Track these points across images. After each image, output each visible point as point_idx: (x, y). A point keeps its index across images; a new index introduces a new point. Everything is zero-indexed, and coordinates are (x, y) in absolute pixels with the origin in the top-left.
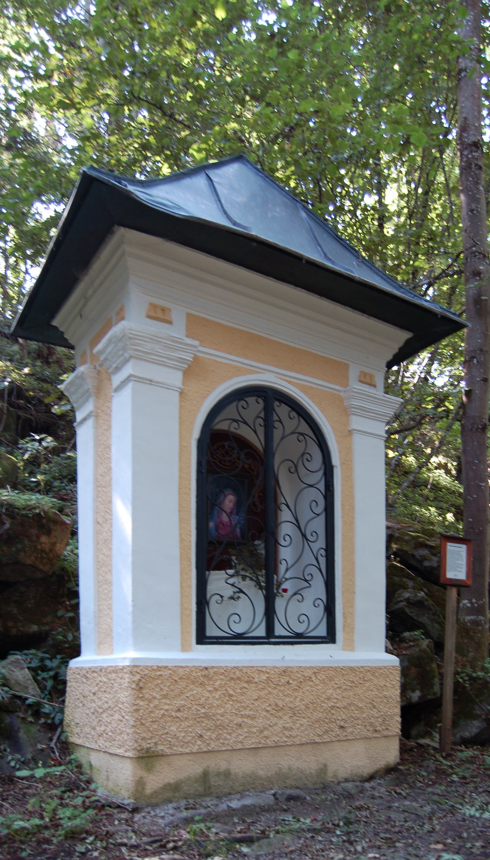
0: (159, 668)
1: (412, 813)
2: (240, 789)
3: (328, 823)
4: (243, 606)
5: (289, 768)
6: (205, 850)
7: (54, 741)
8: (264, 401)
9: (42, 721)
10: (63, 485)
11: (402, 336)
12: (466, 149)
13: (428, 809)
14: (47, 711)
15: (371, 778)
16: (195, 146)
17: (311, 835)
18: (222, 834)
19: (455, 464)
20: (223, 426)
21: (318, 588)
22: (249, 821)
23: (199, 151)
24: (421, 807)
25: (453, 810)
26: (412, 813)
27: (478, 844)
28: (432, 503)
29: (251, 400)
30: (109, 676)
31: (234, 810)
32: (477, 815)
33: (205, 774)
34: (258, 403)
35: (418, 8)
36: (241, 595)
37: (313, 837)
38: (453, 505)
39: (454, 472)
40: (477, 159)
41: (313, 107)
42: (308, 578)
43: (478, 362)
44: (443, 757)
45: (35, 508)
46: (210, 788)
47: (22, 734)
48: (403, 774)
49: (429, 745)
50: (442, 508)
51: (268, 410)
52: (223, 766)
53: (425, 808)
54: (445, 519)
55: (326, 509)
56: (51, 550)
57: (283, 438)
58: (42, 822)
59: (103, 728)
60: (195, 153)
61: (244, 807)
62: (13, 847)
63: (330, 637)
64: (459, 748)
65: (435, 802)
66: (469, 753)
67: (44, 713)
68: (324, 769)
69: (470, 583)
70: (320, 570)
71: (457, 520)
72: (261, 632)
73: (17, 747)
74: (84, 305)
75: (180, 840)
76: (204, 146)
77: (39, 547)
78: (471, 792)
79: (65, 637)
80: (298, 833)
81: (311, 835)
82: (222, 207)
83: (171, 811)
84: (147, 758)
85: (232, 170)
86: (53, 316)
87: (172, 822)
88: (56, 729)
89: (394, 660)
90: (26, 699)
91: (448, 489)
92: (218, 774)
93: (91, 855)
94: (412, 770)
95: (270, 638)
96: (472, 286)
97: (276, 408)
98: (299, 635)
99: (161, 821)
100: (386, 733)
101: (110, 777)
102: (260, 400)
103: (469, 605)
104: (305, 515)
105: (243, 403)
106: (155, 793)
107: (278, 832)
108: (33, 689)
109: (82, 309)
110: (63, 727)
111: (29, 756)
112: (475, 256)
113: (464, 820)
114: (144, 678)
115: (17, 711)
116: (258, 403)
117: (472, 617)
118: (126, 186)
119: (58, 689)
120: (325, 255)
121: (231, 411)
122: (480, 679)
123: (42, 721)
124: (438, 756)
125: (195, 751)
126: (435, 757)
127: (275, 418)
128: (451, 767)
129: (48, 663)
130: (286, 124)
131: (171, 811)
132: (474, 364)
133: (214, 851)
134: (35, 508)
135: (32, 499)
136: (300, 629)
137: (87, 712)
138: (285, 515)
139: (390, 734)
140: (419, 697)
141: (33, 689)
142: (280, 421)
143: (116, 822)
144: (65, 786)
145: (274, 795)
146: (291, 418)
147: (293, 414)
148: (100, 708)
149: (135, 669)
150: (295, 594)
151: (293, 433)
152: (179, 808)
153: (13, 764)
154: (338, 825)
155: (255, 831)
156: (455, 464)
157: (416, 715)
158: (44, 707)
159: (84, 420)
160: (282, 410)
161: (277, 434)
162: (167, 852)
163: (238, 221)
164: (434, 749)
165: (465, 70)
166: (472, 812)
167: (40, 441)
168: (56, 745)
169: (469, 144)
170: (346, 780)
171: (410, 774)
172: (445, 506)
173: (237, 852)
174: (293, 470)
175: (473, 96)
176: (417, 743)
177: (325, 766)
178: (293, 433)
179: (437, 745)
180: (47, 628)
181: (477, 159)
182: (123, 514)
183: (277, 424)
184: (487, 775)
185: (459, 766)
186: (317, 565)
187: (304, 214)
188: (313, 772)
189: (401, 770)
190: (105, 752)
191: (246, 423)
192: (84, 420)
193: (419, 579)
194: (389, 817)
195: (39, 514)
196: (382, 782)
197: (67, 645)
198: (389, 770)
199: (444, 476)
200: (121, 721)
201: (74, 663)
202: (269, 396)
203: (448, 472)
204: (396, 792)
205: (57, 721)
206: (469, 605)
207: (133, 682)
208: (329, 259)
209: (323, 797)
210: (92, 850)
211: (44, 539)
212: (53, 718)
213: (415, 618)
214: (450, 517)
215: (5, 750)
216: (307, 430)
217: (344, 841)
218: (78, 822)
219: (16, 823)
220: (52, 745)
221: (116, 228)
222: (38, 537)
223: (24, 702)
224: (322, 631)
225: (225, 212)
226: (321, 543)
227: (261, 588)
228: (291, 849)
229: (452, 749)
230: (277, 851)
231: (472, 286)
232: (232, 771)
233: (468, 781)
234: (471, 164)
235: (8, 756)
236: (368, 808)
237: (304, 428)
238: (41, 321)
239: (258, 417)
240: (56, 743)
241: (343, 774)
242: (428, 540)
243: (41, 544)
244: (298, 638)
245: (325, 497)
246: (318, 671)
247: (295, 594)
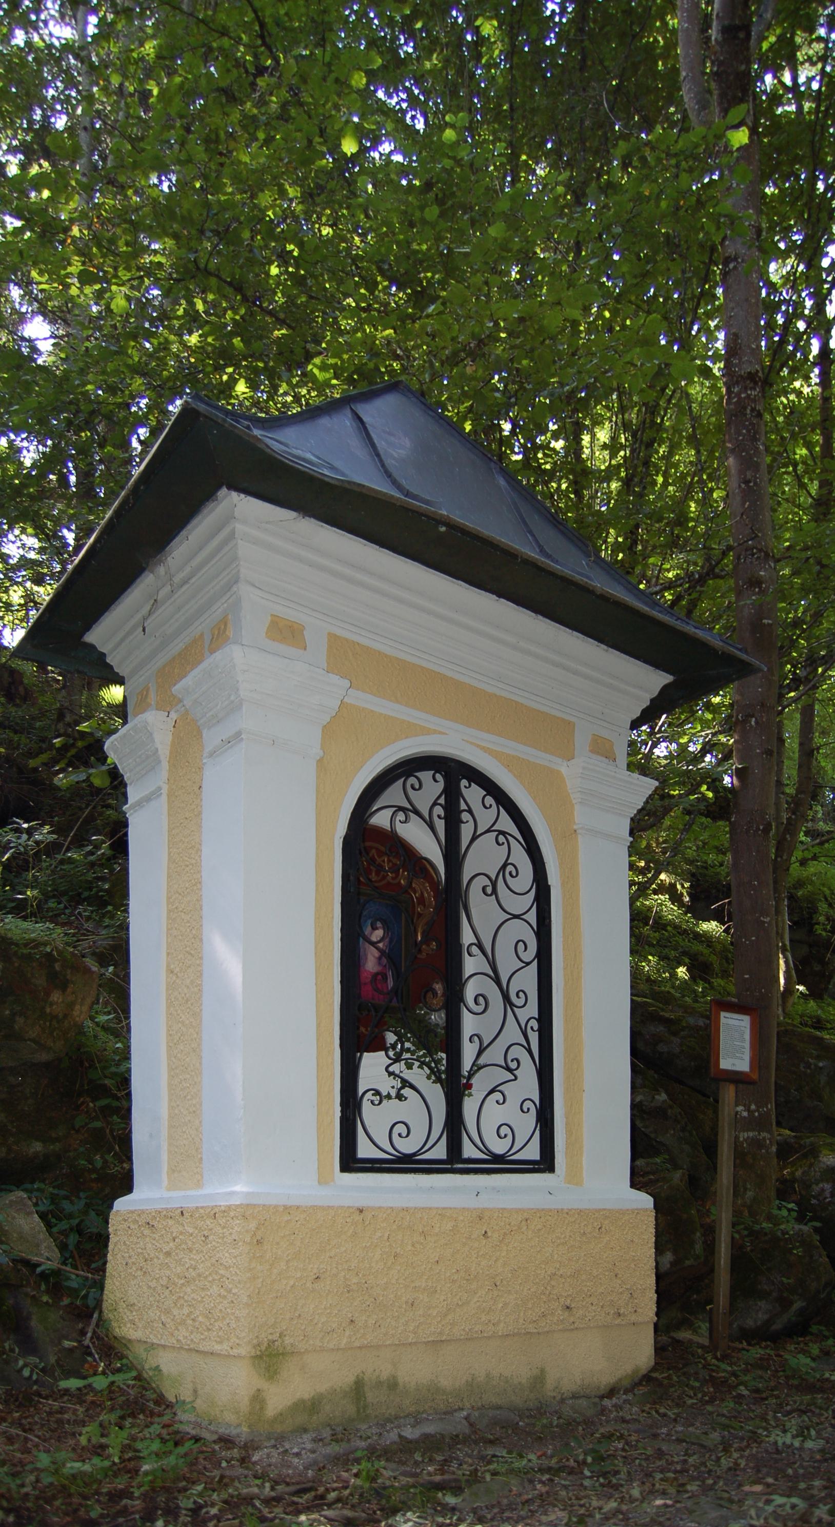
0: (287, 1209)
1: (693, 1444)
2: (412, 1409)
3: (568, 1460)
4: (410, 1110)
5: (488, 1375)
6: (388, 1501)
7: (89, 1335)
8: (445, 778)
9: (66, 1301)
10: (62, 906)
11: (656, 680)
12: (737, 383)
13: (715, 1436)
14: (74, 1285)
15: (612, 1392)
16: (317, 361)
17: (548, 1476)
18: (402, 1478)
19: (687, 885)
20: (381, 819)
22: (440, 1458)
23: (323, 368)
24: (706, 1433)
25: (754, 1437)
26: (693, 1444)
27: (817, 1483)
28: (652, 950)
29: (426, 776)
30: (200, 1223)
31: (410, 1442)
32: (797, 1443)
33: (359, 1386)
34: (436, 781)
35: (673, 162)
36: (406, 1092)
37: (551, 1480)
38: (685, 953)
39: (687, 899)
40: (754, 401)
41: (517, 311)
42: (513, 1065)
43: (757, 723)
44: (718, 1360)
45: (45, 944)
46: (365, 1407)
47: (34, 1323)
48: (661, 1385)
49: (690, 1341)
50: (669, 959)
51: (452, 796)
52: (386, 1371)
53: (711, 1436)
54: (674, 975)
55: (539, 955)
56: (65, 1016)
57: (474, 838)
58: (107, 1463)
59: (186, 1311)
60: (316, 371)
61: (426, 1437)
62: (71, 1504)
64: (737, 1345)
65: (725, 1427)
66: (756, 1352)
67: (69, 1288)
68: (539, 1379)
69: (755, 1077)
70: (530, 1052)
71: (693, 978)
72: (440, 1152)
73: (29, 1345)
74: (150, 613)
75: (346, 1488)
76: (331, 361)
77: (48, 1010)
78: (775, 1412)
79: (90, 1162)
80: (527, 1476)
81: (548, 1476)
82: (383, 465)
83: (309, 1446)
84: (270, 1358)
85: (388, 404)
86: (88, 627)
87: (315, 1462)
88: (91, 1316)
89: (645, 1201)
90: (38, 1265)
91: (676, 927)
92: (379, 1384)
93: (207, 1513)
94: (675, 1378)
95: (454, 1162)
96: (748, 602)
97: (463, 790)
98: (498, 1159)
99: (296, 1460)
100: (633, 1318)
101: (200, 1392)
102: (438, 776)
103: (745, 1114)
104: (506, 963)
105: (412, 780)
106: (280, 1417)
107: (494, 1474)
108: (48, 1247)
109: (145, 619)
110: (101, 1312)
111: (52, 1359)
112: (753, 555)
113: (778, 1452)
114: (264, 1224)
115: (22, 1286)
116: (436, 781)
117: (751, 1134)
118: (248, 428)
119: (92, 1248)
120: (540, 546)
121: (394, 794)
122: (766, 1234)
123: (66, 1301)
124: (709, 1357)
125: (342, 1346)
126: (705, 1359)
127: (463, 806)
128: (734, 1374)
129: (66, 1205)
130: (473, 336)
131: (309, 1446)
132: (751, 726)
133: (403, 1503)
134: (45, 944)
135: (35, 929)
136: (499, 1147)
137: (153, 1284)
138: (471, 964)
139: (640, 1319)
140: (671, 1264)
141: (48, 1247)
142: (470, 811)
143: (224, 1464)
144: (122, 1408)
145: (466, 1418)
146: (485, 807)
147: (489, 800)
148: (179, 1278)
149: (247, 1211)
150: (492, 1091)
151: (488, 831)
152: (321, 1440)
153: (26, 1373)
154: (585, 1462)
155: (461, 1472)
156: (687, 885)
157: (679, 1291)
158: (68, 1279)
159: (148, 799)
160: (472, 794)
161: (466, 832)
162: (330, 1506)
163: (414, 490)
164: (702, 1347)
165: (735, 259)
166: (788, 1439)
167: (30, 832)
168: (93, 1343)
169: (741, 376)
170: (575, 1396)
171: (673, 1386)
172: (673, 954)
173: (440, 1504)
174: (489, 890)
175: (747, 300)
176: (673, 1338)
177: (542, 1371)
178: (488, 831)
179: (706, 1342)
180: (57, 1147)
181: (754, 401)
182: (227, 959)
183: (465, 816)
185: (746, 1371)
187: (502, 482)
188: (524, 1381)
189: (656, 1379)
190: (190, 1350)
192: (148, 799)
193: (651, 1073)
194: (659, 1449)
195: (49, 955)
196: (630, 1397)
197: (93, 1176)
198: (647, 1378)
199: (669, 903)
200: (225, 1297)
201: (121, 1204)
202: (454, 772)
203: (675, 898)
204: (657, 1412)
205: (91, 1302)
206: (745, 1114)
207: (247, 1231)
208: (548, 556)
209: (545, 1421)
210: (206, 1505)
211: (56, 996)
212: (85, 1297)
213: (653, 1136)
214: (682, 971)
215: (12, 1350)
216: (512, 829)
217: (602, 1485)
218: (172, 1460)
219: (69, 1465)
220: (87, 1342)
221: (224, 491)
222: (48, 994)
223: (34, 1272)
224: (533, 1152)
225: (389, 475)
226: (533, 1009)
227: (438, 1080)
228: (526, 1497)
229: (729, 1348)
230: (505, 1501)
231: (748, 602)
232: (400, 1381)
233: (764, 1395)
234: (745, 408)
235: (17, 1360)
236: (622, 1436)
237: (506, 823)
238: (62, 631)
239: (435, 804)
240: (92, 1338)
241: (568, 1386)
242: (663, 1010)
243: (51, 1004)
244: (498, 1164)
245: (538, 934)
246: (527, 1217)
247: (492, 1091)
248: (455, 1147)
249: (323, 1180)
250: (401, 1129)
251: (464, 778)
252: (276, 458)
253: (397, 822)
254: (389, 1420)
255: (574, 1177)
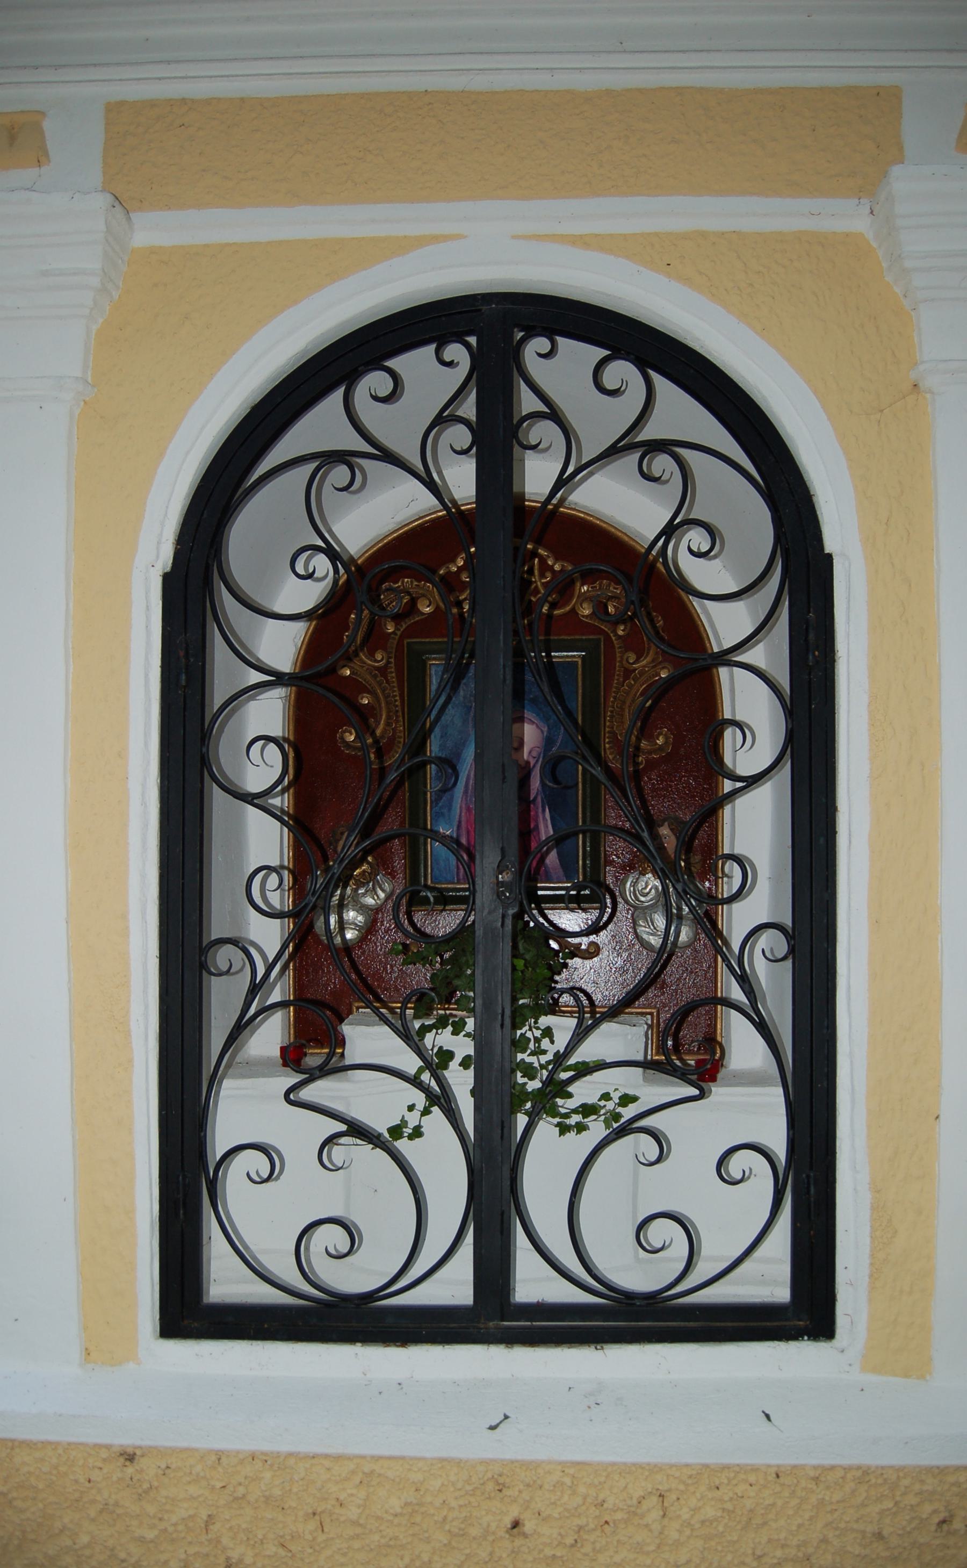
21: (752, 1108)
51: (496, 377)
63: (809, 1312)
72: (455, 1286)
127: (528, 402)
142: (554, 415)
151: (613, 451)
160: (561, 370)
178: (613, 451)
184: (645, 945)
186: (320, 543)
191: (388, 457)
237: (680, 413)
239: (442, 420)
248: (493, 1271)
249: (100, 1349)
250: (333, 1237)
251: (531, 332)
252: (295, 1032)
253: (327, 490)
254: (472, 857)
255: (905, 1352)
